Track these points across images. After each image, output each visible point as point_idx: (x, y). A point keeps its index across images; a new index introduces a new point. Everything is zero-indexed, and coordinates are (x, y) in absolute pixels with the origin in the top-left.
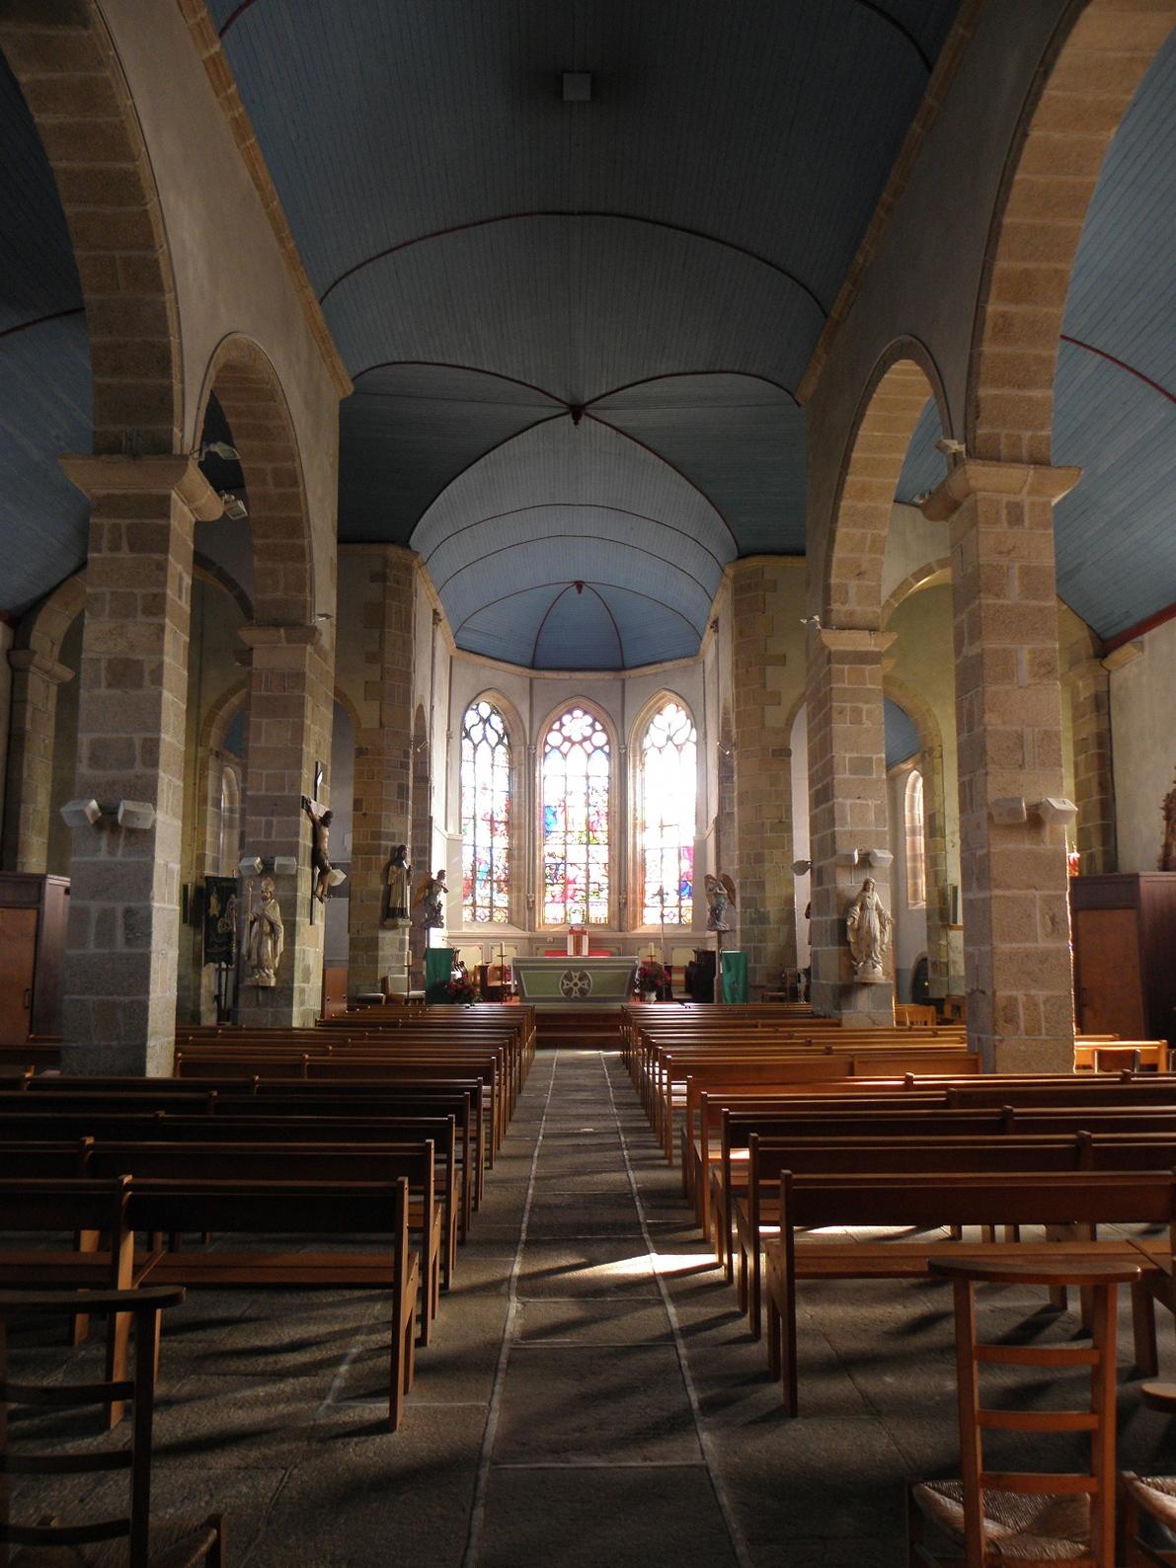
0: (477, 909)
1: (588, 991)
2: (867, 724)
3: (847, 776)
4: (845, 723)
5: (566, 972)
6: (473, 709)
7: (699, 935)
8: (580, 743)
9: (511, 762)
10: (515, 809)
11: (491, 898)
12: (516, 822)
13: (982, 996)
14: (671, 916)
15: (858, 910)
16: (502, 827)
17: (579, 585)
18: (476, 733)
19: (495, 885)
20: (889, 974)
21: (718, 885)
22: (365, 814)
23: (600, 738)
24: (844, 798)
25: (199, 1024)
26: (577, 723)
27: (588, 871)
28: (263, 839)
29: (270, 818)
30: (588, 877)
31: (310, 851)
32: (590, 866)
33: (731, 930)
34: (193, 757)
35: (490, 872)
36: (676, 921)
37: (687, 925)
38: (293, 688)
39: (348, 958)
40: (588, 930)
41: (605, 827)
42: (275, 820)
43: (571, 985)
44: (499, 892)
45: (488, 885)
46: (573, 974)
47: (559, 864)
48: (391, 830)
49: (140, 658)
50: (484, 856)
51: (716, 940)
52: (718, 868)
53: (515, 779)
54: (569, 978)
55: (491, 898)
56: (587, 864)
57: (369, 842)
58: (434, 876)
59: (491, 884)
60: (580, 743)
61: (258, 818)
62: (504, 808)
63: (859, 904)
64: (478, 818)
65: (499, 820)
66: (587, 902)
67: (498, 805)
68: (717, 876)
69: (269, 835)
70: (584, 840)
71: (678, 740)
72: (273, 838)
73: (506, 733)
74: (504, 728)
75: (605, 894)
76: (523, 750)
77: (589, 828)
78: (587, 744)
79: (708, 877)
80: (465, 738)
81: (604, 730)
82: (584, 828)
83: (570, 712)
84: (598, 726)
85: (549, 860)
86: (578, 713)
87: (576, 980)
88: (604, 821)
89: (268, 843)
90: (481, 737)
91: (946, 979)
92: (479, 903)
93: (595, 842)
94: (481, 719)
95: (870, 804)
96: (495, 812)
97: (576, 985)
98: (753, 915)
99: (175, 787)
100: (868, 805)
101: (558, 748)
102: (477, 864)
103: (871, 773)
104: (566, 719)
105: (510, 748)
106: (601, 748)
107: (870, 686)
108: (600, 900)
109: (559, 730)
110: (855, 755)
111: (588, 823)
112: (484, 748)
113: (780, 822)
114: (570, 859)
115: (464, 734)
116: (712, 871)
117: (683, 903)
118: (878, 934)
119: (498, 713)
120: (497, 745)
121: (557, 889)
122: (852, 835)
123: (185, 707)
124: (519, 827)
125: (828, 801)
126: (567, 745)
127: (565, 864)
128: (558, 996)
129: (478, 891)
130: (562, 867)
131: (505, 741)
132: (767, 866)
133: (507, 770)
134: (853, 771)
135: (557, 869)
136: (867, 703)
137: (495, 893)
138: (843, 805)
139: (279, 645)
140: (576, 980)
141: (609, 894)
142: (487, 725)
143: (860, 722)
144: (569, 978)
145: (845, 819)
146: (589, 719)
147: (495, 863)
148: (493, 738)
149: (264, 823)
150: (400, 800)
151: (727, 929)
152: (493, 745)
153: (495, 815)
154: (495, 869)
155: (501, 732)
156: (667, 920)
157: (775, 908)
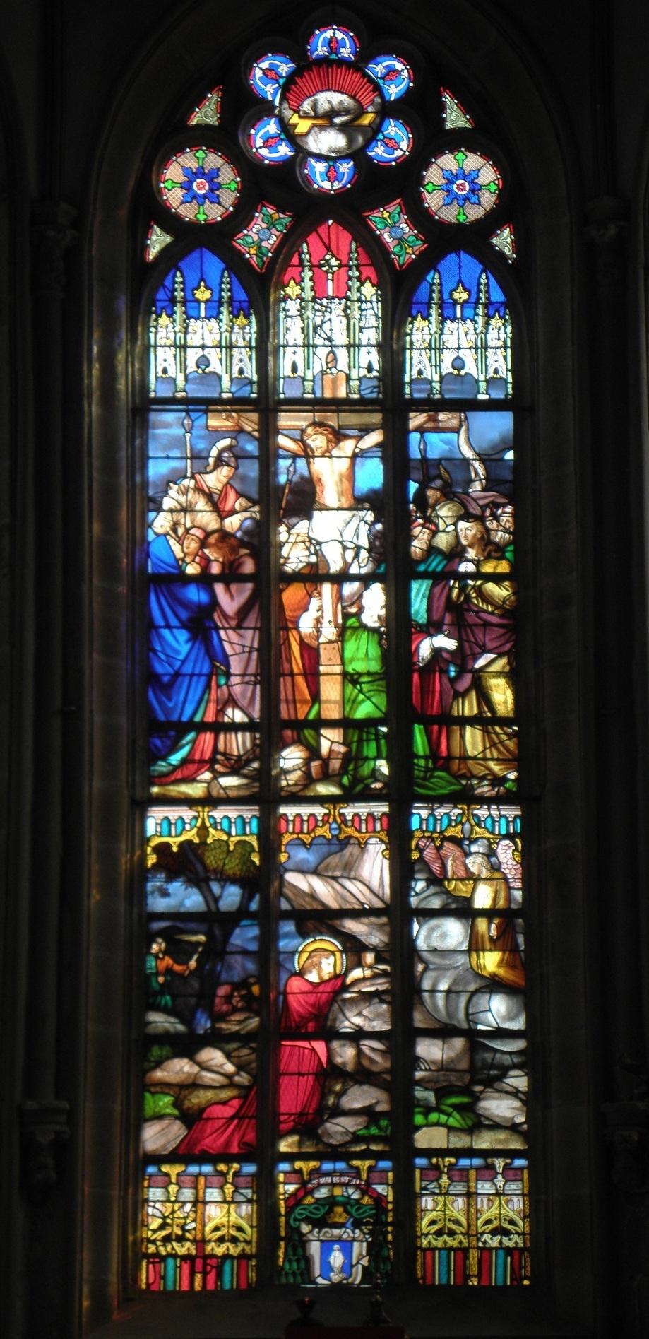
93: (442, 782)
108: (485, 1141)
127: (268, 919)
130: (246, 936)
135: (216, 951)
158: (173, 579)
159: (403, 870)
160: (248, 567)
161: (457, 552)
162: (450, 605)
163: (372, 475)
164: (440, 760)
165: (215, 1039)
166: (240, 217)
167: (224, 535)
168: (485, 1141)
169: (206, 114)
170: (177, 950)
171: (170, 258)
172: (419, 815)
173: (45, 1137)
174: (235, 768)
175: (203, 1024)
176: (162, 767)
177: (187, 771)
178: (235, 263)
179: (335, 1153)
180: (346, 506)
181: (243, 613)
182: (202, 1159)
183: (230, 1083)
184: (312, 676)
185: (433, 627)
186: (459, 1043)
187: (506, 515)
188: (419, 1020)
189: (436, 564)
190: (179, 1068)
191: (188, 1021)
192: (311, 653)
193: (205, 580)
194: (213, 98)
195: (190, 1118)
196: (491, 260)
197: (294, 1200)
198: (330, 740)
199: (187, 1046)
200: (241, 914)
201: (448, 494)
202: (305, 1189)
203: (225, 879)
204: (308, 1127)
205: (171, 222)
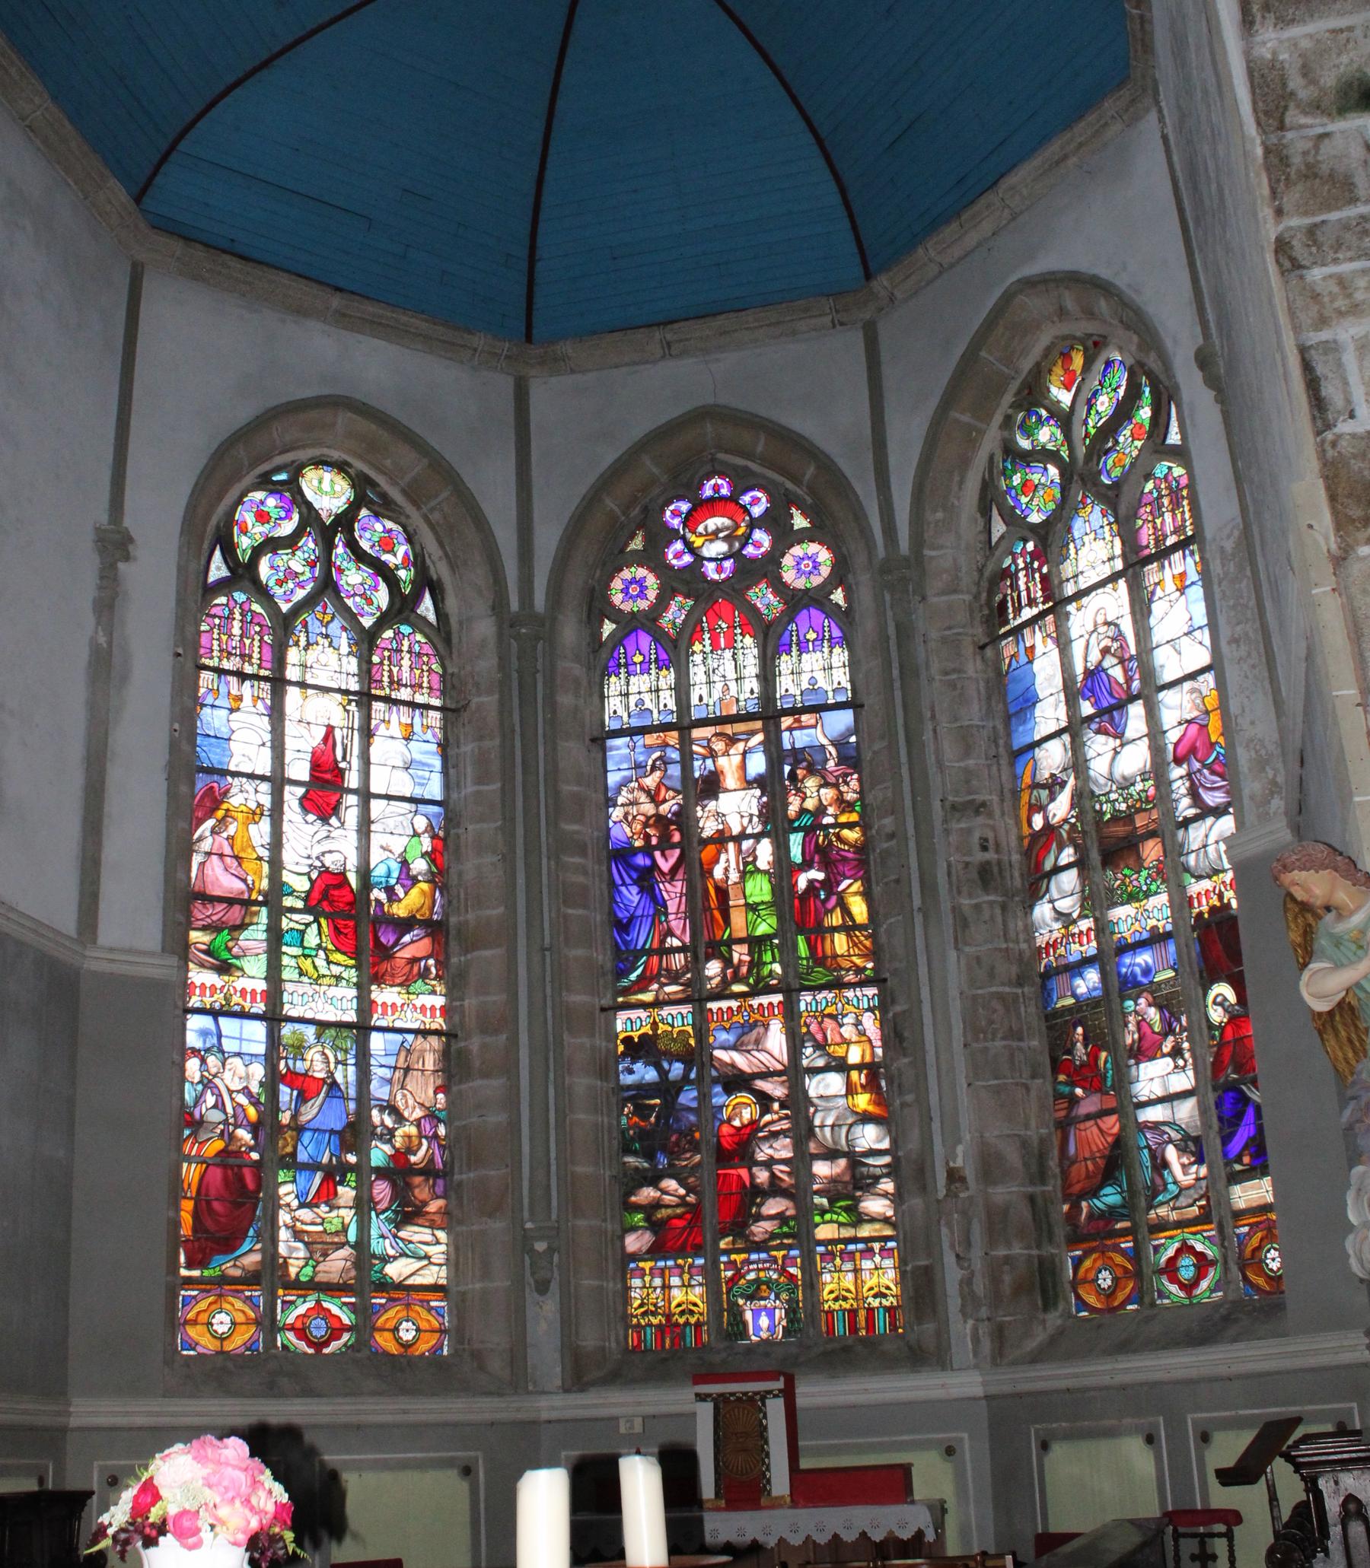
27: (798, 1103)
30: (802, 1131)
41: (859, 909)
47: (678, 1087)
55: (362, 1245)
78: (764, 599)
93: (820, 976)
101: (648, 621)
102: (285, 1093)
106: (815, 599)
108: (865, 1231)
130: (688, 1097)
137: (378, 1225)
141: (897, 1198)
147: (378, 1090)
161: (821, 810)
168: (865, 1231)
170: (642, 1111)
174: (674, 977)
175: (663, 1161)
177: (642, 984)
181: (674, 870)
186: (842, 1162)
189: (806, 820)
190: (647, 1194)
193: (648, 850)
195: (654, 1225)
197: (732, 1281)
201: (811, 771)
202: (739, 1275)
203: (674, 1057)
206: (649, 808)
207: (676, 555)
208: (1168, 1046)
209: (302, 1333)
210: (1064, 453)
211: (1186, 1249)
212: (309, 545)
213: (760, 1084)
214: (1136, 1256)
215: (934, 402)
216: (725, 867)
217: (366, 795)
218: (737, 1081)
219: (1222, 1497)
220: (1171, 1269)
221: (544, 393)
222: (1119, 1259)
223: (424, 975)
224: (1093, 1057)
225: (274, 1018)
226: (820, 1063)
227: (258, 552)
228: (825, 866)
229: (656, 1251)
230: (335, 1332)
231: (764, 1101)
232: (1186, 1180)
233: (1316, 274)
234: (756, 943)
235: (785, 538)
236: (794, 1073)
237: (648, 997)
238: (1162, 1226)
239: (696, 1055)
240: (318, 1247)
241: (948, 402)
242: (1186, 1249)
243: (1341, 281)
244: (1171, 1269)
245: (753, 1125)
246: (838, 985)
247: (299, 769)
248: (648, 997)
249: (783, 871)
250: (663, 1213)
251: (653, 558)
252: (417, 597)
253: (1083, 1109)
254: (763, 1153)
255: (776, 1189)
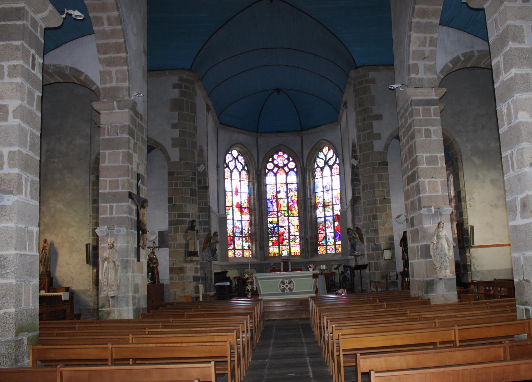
0: (236, 251)
1: (293, 289)
2: (434, 137)
3: (425, 166)
4: (422, 138)
5: (281, 280)
6: (230, 154)
7: (345, 258)
8: (282, 168)
9: (249, 178)
10: (252, 202)
11: (242, 245)
12: (253, 207)
13: (527, 283)
14: (331, 250)
15: (436, 239)
16: (246, 210)
17: (278, 90)
18: (232, 165)
19: (244, 239)
20: (453, 272)
21: (354, 233)
22: (174, 205)
23: (292, 165)
24: (424, 178)
25: (163, 300)
26: (280, 159)
27: (289, 229)
28: (108, 215)
29: (112, 204)
30: (289, 232)
31: (136, 222)
32: (290, 227)
33: (362, 255)
34: (88, 180)
35: (241, 233)
36: (333, 252)
37: (339, 254)
38: (121, 133)
39: (169, 278)
40: (291, 259)
41: (297, 208)
42: (115, 205)
43: (285, 286)
44: (246, 242)
45: (241, 239)
46: (285, 281)
47: (275, 227)
48: (188, 213)
49: (6, 103)
50: (238, 224)
51: (354, 260)
52: (354, 225)
53: (251, 186)
54: (283, 283)
55: (242, 245)
56: (289, 226)
57: (177, 219)
58: (212, 235)
59: (242, 239)
60: (282, 168)
61: (106, 204)
62: (246, 201)
63: (436, 235)
64: (234, 206)
65: (244, 207)
66: (289, 245)
67: (243, 199)
68: (353, 228)
69: (111, 213)
70: (287, 214)
71: (331, 163)
72: (114, 215)
73: (246, 164)
74: (245, 162)
75: (298, 241)
76: (255, 172)
77: (289, 208)
78: (286, 169)
79: (348, 229)
80: (226, 168)
81: (293, 161)
82: (286, 209)
83: (277, 153)
84: (291, 159)
85: (270, 225)
86: (281, 153)
87: (287, 284)
88: (296, 205)
89: (111, 218)
90: (234, 167)
91: (470, 273)
92: (237, 248)
93: (292, 215)
94: (234, 158)
95: (438, 181)
96: (242, 202)
97: (287, 286)
98: (373, 246)
99: (32, 181)
100: (437, 182)
101: (272, 170)
102: (235, 228)
103: (438, 164)
104: (275, 156)
105: (248, 172)
106: (293, 170)
107: (434, 118)
108: (296, 244)
109: (272, 162)
110: (429, 155)
111: (288, 206)
112: (235, 172)
113: (385, 198)
114: (280, 224)
115: (225, 166)
116: (350, 225)
117: (337, 243)
118: (447, 251)
119: (242, 155)
120: (242, 170)
121: (275, 239)
122: (429, 197)
123: (39, 134)
124: (255, 210)
125: (415, 180)
126: (276, 170)
127: (278, 227)
128: (278, 292)
129: (236, 242)
130: (276, 228)
131: (246, 168)
132: (379, 221)
133: (247, 182)
134: (428, 163)
135: (274, 230)
136: (433, 126)
137: (244, 243)
138: (424, 182)
139: (114, 111)
140: (287, 284)
141: (300, 240)
142: (237, 161)
143: (430, 137)
144: (283, 283)
145: (425, 189)
146: (286, 156)
147: (243, 228)
148: (240, 167)
149: (108, 207)
150: (191, 197)
151: (360, 254)
152: (240, 171)
153: (242, 205)
154: (244, 231)
155: (244, 164)
156: (329, 252)
157: (384, 243)
158: (269, 199)
159: (289, 223)
160: (275, 198)
161: (292, 196)
162: (292, 201)
163: (285, 190)
164: (292, 214)
165: (274, 237)
166: (274, 169)
167: (273, 195)
168: (296, 244)
169: (270, 160)
170: (271, 230)
171: (268, 172)
172: (290, 218)
173: (262, 245)
174: (275, 215)
175: (273, 236)
176: (269, 215)
177: (271, 215)
178: (273, 172)
179: (284, 245)
180: (320, 218)
181: (275, 202)
182: (274, 246)
183: (276, 240)
184: (281, 207)
185: (291, 202)
186: (294, 236)
187: (296, 192)
188: (290, 235)
189: (291, 197)
190: (271, 239)
191: (272, 235)
192: (281, 205)
193: (272, 199)
194: (271, 159)
195: (273, 243)
196: (294, 171)
197: (281, 249)
198: (283, 212)
199: (272, 237)
200: (276, 227)
201: (291, 191)
202: (282, 248)
203: (274, 224)
204: (282, 243)
205: (268, 169)
206: (272, 194)
207: (275, 162)
208: (331, 227)
209: (237, 255)
210: (325, 159)
211: (331, 248)
212: (234, 161)
213: (284, 227)
214: (326, 248)
215: (310, 150)
216: (281, 202)
217: (241, 193)
218: (282, 227)
219: (334, 271)
220: (329, 250)
221: (260, 140)
222: (324, 248)
223: (247, 214)
224: (323, 227)
225: (233, 220)
226: (292, 225)
227: (228, 163)
228: (293, 202)
229: (272, 246)
230: (240, 254)
231: (285, 229)
232: (332, 241)
233: (354, 183)
234: (284, 211)
235: (289, 161)
236: (289, 226)
237: (272, 217)
238: (329, 245)
239: (278, 224)
240: (239, 245)
241: (311, 150)
242: (331, 248)
243: (356, 183)
244: (329, 250)
245: (284, 232)
246: (294, 216)
247: (234, 190)
248: (272, 217)
249: (288, 203)
250: (273, 241)
251: (272, 162)
252: (245, 167)
253: (321, 233)
254: (285, 235)
255: (286, 239)
